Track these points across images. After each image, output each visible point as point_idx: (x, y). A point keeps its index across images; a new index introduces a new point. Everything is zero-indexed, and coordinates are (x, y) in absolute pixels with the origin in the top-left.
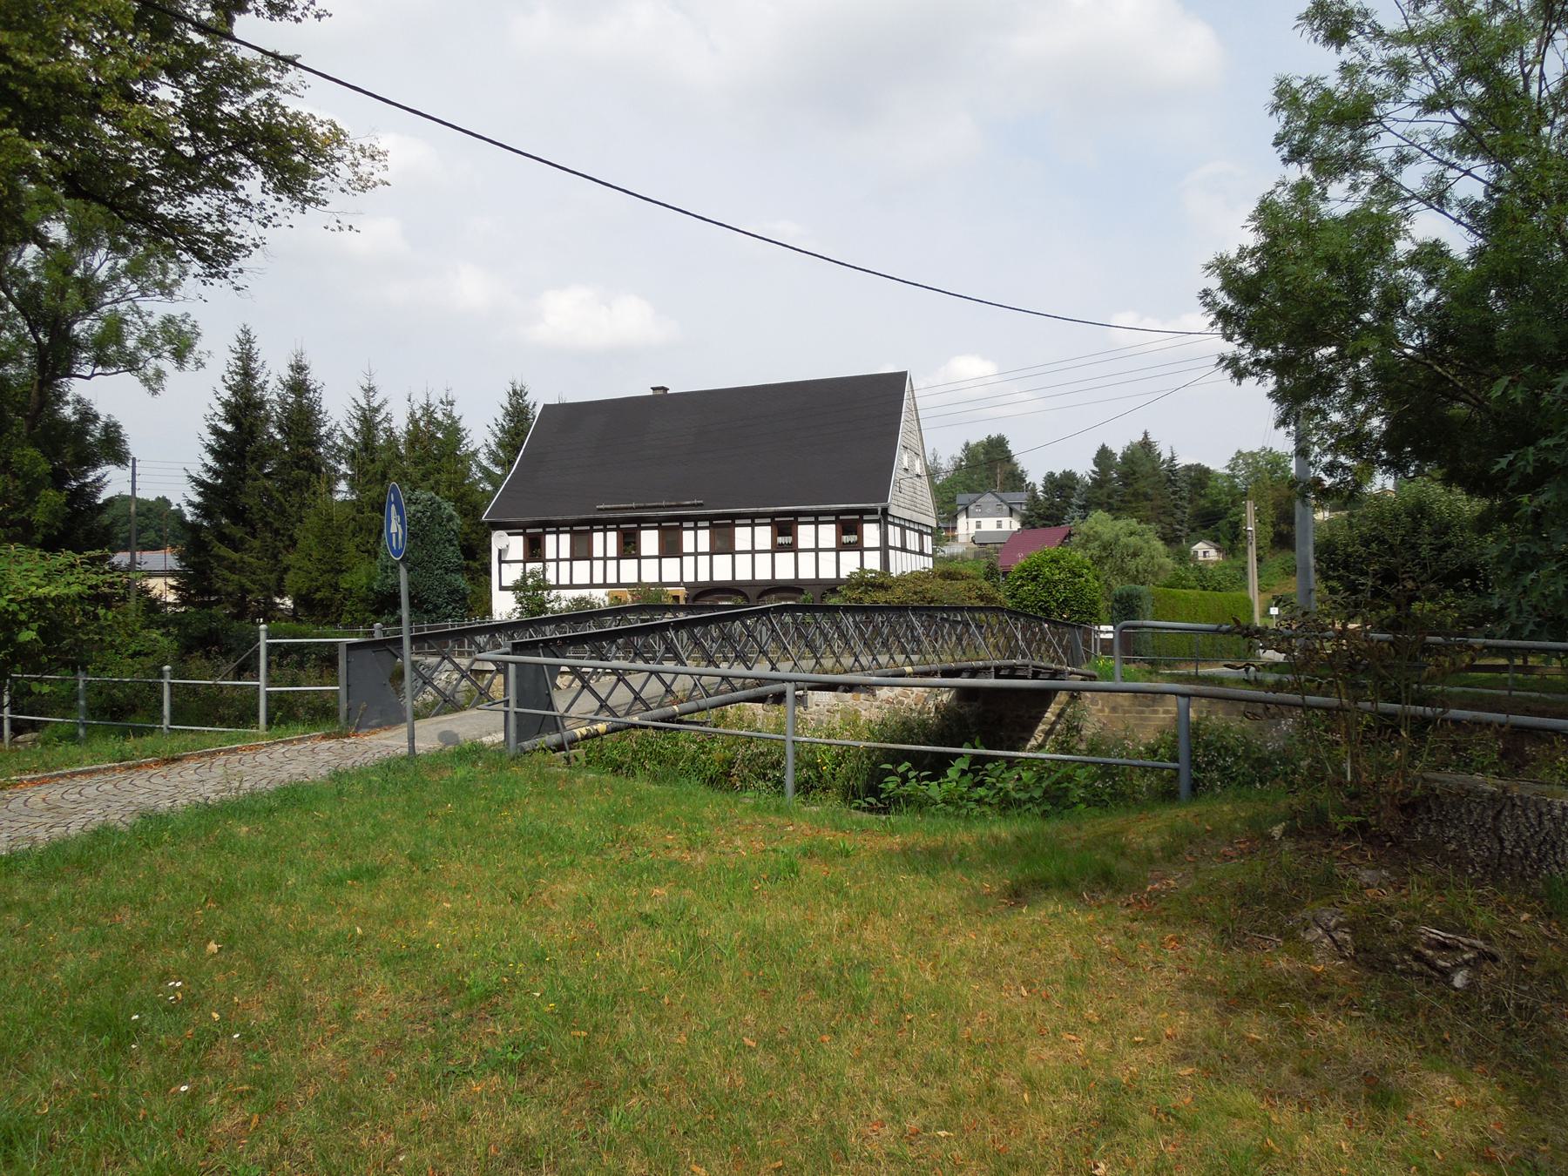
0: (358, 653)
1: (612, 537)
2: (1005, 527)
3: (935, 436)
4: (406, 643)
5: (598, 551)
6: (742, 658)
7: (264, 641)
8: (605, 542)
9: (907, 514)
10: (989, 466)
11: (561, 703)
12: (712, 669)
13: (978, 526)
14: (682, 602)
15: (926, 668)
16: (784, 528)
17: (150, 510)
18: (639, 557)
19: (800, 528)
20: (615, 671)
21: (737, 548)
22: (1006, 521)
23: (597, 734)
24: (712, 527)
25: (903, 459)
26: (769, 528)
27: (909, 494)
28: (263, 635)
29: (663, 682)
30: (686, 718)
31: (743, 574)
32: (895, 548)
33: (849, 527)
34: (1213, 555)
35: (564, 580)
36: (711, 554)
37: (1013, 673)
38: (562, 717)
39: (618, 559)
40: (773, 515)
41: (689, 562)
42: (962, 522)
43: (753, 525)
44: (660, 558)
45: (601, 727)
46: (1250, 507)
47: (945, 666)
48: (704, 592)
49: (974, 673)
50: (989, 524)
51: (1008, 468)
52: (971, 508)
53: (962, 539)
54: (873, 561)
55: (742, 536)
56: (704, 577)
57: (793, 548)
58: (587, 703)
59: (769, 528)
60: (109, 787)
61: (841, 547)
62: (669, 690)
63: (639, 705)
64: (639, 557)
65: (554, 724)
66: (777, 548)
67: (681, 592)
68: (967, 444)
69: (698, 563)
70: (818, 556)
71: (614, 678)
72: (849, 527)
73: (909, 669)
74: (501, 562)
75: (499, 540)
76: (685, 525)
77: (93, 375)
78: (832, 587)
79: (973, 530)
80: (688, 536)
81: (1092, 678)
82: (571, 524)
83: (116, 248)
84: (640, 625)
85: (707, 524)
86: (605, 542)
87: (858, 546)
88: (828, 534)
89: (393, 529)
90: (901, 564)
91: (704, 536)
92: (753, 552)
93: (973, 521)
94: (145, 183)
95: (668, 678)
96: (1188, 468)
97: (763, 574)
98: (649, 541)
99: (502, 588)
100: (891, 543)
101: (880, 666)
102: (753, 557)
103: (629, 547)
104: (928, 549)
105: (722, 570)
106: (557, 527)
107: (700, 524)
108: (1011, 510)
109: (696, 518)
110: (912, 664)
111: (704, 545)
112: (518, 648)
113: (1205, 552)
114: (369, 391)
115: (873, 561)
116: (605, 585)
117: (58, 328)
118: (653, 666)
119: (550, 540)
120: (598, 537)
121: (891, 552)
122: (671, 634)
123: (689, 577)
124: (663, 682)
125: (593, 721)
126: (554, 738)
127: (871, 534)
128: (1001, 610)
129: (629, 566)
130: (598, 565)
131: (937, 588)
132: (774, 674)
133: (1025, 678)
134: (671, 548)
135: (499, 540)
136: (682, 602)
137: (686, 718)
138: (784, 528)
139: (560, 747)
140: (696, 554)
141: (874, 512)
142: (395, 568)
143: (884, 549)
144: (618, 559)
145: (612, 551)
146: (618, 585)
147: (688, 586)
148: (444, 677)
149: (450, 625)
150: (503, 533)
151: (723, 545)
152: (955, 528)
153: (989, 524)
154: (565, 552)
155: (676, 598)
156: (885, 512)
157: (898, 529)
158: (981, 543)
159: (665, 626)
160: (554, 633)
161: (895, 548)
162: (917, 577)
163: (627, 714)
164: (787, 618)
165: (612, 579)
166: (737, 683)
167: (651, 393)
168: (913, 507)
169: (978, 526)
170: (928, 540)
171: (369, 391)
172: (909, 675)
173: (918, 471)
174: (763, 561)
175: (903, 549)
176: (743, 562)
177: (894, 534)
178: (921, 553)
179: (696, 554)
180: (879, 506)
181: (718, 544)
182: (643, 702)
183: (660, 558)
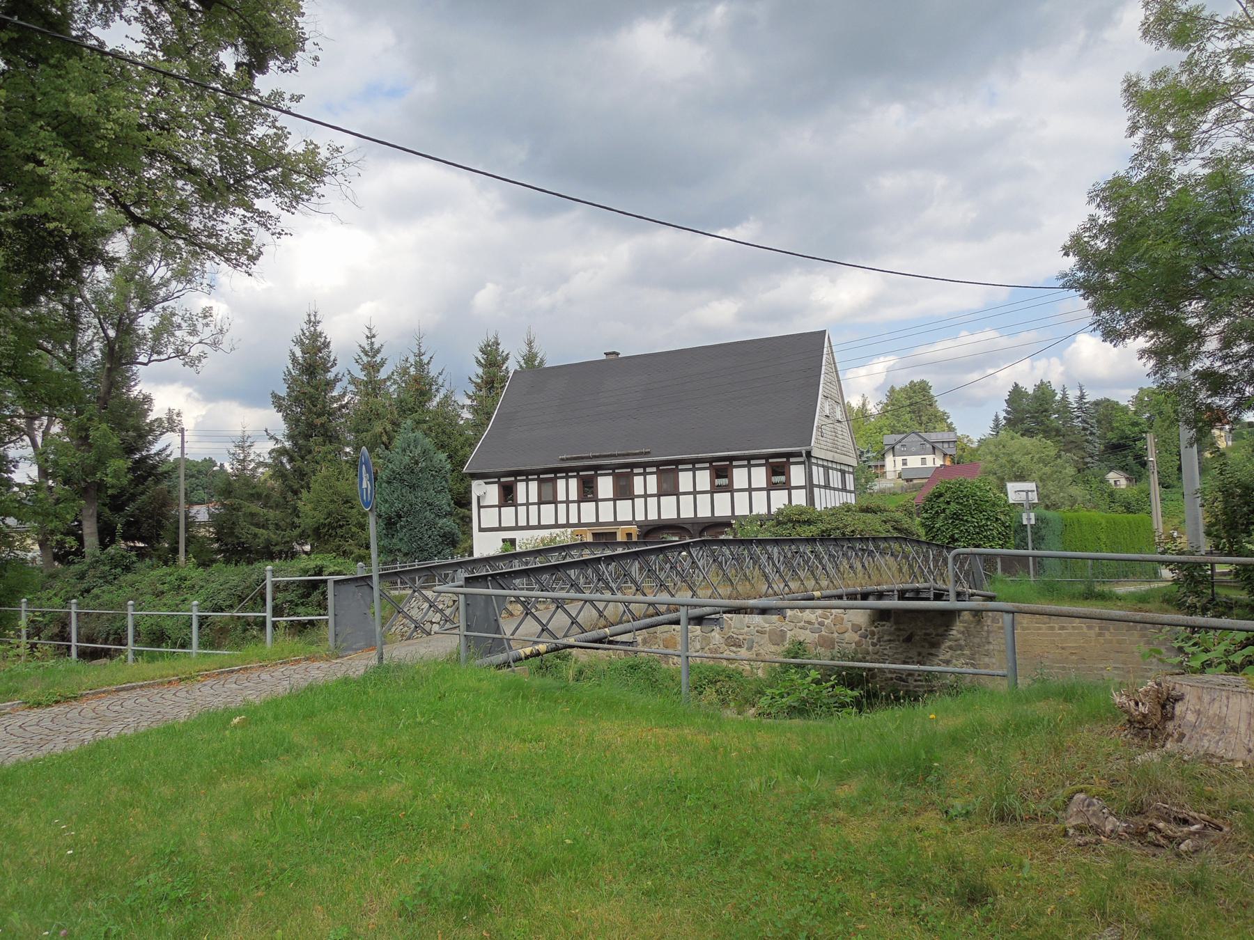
0: (343, 587)
1: (573, 483)
2: (930, 464)
3: (863, 383)
4: (375, 579)
5: (561, 496)
6: (662, 586)
7: (269, 580)
8: (568, 488)
9: (829, 456)
10: (914, 408)
11: (507, 627)
12: (640, 597)
13: (905, 464)
14: (635, 539)
15: (834, 592)
16: (721, 471)
17: (199, 472)
18: (596, 500)
19: (793, 468)
20: (554, 600)
21: (735, 487)
22: (929, 458)
23: (538, 654)
24: (541, 481)
25: (823, 406)
26: (764, 469)
27: (829, 438)
28: (269, 575)
29: (598, 610)
30: (618, 638)
31: (687, 513)
32: (819, 486)
33: (778, 469)
34: (1123, 483)
35: (534, 522)
36: (659, 496)
37: (917, 595)
38: (509, 640)
39: (579, 502)
40: (767, 457)
41: (639, 502)
42: (889, 459)
43: (749, 466)
44: (500, 507)
45: (542, 648)
46: (1150, 440)
47: (851, 590)
48: (651, 530)
49: (880, 595)
50: (914, 462)
51: (931, 410)
52: (897, 447)
53: (890, 476)
54: (799, 498)
55: (685, 481)
56: (653, 516)
57: (729, 489)
58: (531, 627)
59: (764, 469)
60: (144, 700)
61: (771, 487)
62: (601, 614)
63: (575, 629)
64: (596, 500)
65: (499, 645)
66: (715, 489)
67: (634, 529)
68: (892, 390)
69: (650, 504)
70: (751, 497)
71: (553, 607)
72: (778, 469)
73: (817, 594)
74: (480, 507)
75: (478, 488)
76: (636, 471)
77: (150, 361)
78: (723, 524)
79: (899, 467)
80: (638, 481)
81: (991, 598)
82: (538, 472)
83: (168, 255)
84: (602, 556)
85: (654, 469)
86: (568, 488)
87: (786, 486)
88: (760, 476)
89: (364, 486)
90: (826, 500)
91: (652, 480)
92: (750, 490)
93: (899, 459)
94: (183, 207)
95: (601, 606)
96: (1097, 403)
97: (704, 512)
98: (605, 485)
99: (481, 530)
100: (815, 482)
101: (791, 592)
102: (694, 498)
103: (588, 491)
104: (850, 485)
105: (668, 510)
106: (526, 474)
107: (648, 470)
108: (934, 448)
109: (644, 465)
110: (821, 589)
111: (653, 487)
112: (469, 581)
113: (1117, 479)
114: (530, 344)
115: (799, 498)
116: (568, 525)
117: (126, 327)
118: (587, 595)
119: (521, 487)
120: (561, 484)
121: (816, 490)
122: (602, 567)
123: (640, 517)
124: (598, 610)
125: (536, 643)
126: (500, 658)
127: (797, 474)
128: (918, 542)
129: (588, 509)
130: (522, 510)
131: (858, 523)
132: (695, 600)
133: (928, 599)
134: (624, 491)
135: (478, 488)
136: (635, 539)
137: (618, 638)
138: (721, 471)
139: (507, 664)
140: (646, 496)
141: (799, 455)
142: (365, 515)
143: (810, 487)
144: (579, 502)
145: (574, 495)
146: (579, 525)
147: (640, 525)
148: (417, 609)
149: (436, 562)
150: (481, 482)
151: (669, 488)
152: (883, 466)
153: (914, 462)
154: (534, 498)
155: (629, 535)
156: (809, 454)
157: (821, 469)
158: (907, 477)
159: (598, 560)
160: (509, 569)
161: (819, 486)
162: (834, 512)
163: (565, 636)
164: (775, 551)
165: (573, 520)
166: (663, 608)
167: (604, 357)
168: (835, 448)
169: (905, 464)
170: (850, 479)
171: (530, 344)
172: (819, 599)
173: (839, 417)
174: (704, 500)
175: (827, 486)
176: (687, 501)
177: (818, 475)
178: (844, 489)
179: (646, 496)
180: (803, 450)
181: (665, 486)
182: (579, 626)
183: (500, 507)
